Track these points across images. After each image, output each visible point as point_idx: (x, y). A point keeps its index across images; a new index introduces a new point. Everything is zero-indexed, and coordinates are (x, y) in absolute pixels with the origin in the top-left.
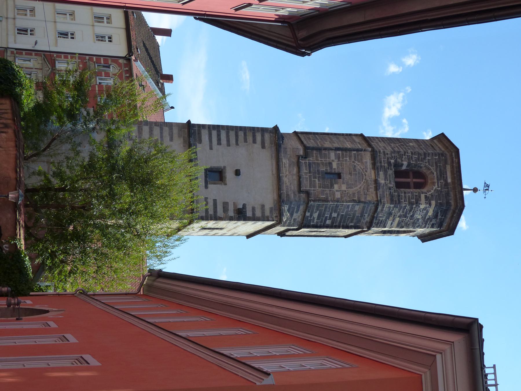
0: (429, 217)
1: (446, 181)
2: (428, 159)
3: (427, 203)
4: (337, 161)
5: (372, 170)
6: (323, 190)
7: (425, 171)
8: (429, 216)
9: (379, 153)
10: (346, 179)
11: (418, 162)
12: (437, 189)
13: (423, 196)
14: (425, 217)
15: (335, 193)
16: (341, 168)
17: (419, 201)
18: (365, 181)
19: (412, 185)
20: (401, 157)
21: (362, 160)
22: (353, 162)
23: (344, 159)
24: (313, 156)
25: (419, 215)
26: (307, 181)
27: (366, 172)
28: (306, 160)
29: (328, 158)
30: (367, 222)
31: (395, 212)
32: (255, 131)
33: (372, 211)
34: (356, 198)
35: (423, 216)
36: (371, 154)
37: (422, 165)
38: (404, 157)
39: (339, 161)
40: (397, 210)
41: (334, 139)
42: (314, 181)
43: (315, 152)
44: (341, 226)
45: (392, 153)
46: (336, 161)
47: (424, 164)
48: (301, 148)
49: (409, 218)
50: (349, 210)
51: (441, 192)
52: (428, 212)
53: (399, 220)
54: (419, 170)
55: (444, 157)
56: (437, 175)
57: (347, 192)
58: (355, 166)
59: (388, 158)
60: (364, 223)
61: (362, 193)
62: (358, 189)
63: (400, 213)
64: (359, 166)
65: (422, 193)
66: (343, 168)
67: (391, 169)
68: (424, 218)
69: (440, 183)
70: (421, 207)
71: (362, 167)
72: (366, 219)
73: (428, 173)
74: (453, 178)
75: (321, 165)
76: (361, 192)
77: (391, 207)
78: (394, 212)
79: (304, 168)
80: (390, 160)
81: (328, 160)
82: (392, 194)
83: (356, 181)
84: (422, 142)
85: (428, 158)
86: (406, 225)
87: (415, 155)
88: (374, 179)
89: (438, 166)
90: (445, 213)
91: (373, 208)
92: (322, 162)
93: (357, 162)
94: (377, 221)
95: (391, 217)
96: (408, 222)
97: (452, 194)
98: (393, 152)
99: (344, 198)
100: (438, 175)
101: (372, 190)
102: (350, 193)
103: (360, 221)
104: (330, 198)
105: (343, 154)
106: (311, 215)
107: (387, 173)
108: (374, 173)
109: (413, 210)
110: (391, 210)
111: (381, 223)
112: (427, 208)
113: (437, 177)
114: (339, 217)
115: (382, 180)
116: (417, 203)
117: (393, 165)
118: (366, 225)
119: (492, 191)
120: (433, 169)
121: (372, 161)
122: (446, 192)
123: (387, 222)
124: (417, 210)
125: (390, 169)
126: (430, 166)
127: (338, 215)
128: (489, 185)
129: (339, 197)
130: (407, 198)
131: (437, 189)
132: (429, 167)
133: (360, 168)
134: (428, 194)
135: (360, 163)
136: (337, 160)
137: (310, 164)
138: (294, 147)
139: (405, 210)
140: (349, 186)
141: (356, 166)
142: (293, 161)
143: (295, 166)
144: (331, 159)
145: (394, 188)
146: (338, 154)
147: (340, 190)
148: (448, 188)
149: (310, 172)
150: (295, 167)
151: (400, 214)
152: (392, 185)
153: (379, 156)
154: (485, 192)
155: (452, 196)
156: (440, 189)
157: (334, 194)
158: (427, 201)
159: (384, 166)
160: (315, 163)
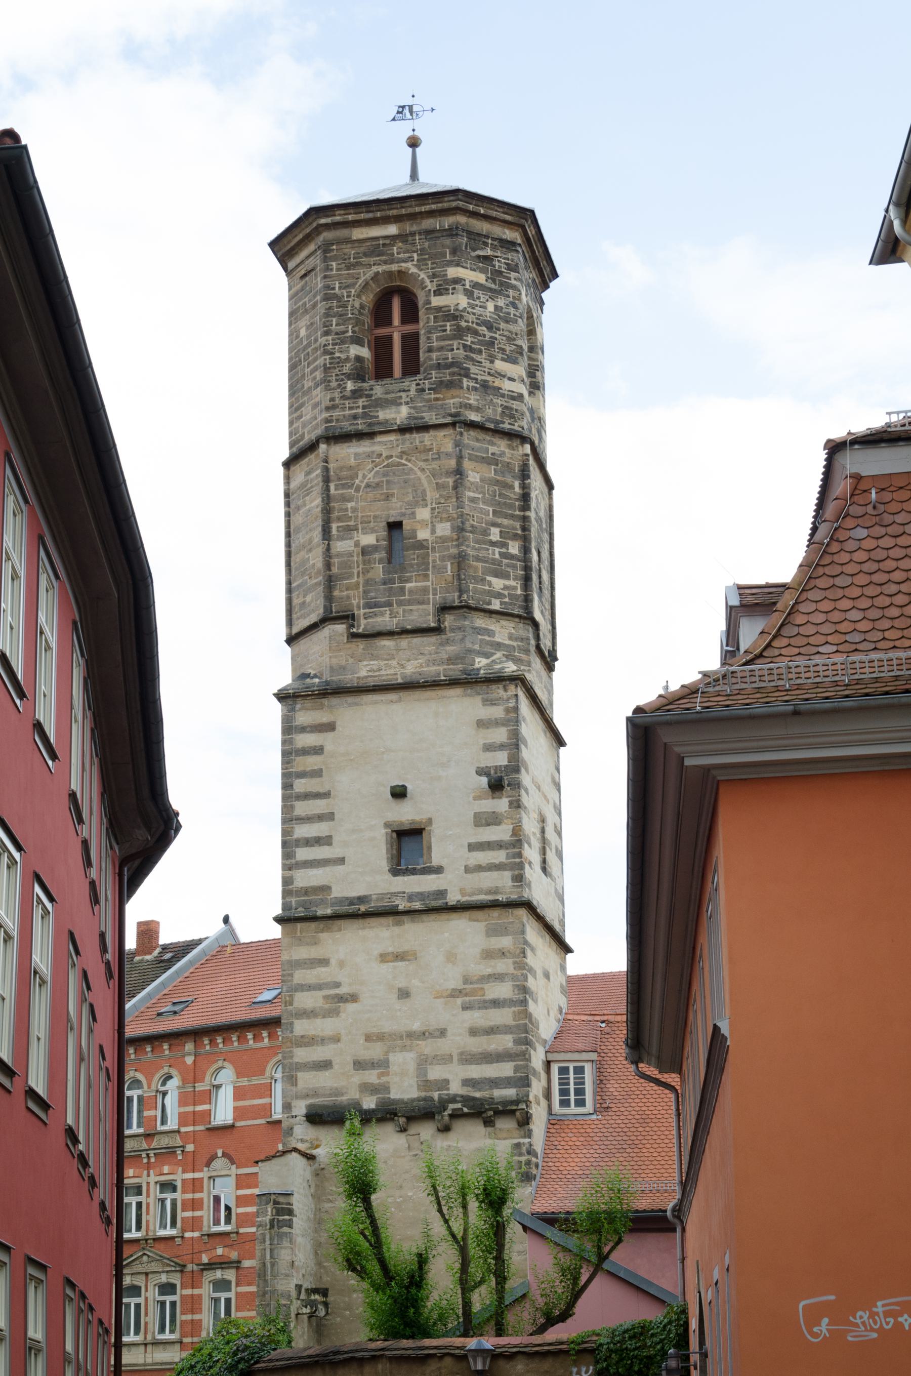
2: (340, 288)
3: (454, 289)
9: (331, 421)
11: (350, 316)
12: (415, 263)
13: (436, 301)
14: (491, 290)
15: (440, 537)
17: (450, 311)
19: (409, 328)
20: (338, 363)
24: (348, 597)
29: (351, 559)
30: (510, 447)
34: (450, 481)
37: (357, 305)
38: (337, 355)
39: (357, 529)
41: (299, 539)
43: (336, 593)
44: (522, 513)
47: (354, 300)
50: (480, 496)
51: (422, 252)
52: (476, 285)
56: (379, 264)
57: (434, 505)
58: (368, 486)
59: (344, 398)
60: (512, 455)
61: (435, 465)
65: (428, 302)
66: (375, 517)
68: (494, 294)
69: (401, 256)
71: (370, 466)
75: (370, 575)
80: (348, 393)
81: (355, 558)
82: (435, 386)
85: (337, 289)
89: (357, 263)
92: (363, 573)
95: (494, 382)
96: (505, 336)
98: (326, 386)
100: (380, 260)
102: (437, 496)
105: (339, 519)
106: (499, 595)
107: (381, 398)
109: (474, 325)
110: (476, 385)
113: (385, 262)
114: (499, 521)
115: (399, 412)
116: (455, 317)
123: (506, 393)
124: (474, 314)
125: (371, 392)
126: (359, 284)
127: (495, 525)
128: (400, 107)
134: (429, 287)
137: (368, 606)
138: (328, 648)
139: (473, 346)
141: (367, 483)
144: (352, 548)
145: (420, 380)
146: (338, 531)
149: (389, 604)
151: (485, 359)
153: (337, 420)
156: (415, 255)
157: (443, 539)
158: (447, 289)
159: (364, 407)
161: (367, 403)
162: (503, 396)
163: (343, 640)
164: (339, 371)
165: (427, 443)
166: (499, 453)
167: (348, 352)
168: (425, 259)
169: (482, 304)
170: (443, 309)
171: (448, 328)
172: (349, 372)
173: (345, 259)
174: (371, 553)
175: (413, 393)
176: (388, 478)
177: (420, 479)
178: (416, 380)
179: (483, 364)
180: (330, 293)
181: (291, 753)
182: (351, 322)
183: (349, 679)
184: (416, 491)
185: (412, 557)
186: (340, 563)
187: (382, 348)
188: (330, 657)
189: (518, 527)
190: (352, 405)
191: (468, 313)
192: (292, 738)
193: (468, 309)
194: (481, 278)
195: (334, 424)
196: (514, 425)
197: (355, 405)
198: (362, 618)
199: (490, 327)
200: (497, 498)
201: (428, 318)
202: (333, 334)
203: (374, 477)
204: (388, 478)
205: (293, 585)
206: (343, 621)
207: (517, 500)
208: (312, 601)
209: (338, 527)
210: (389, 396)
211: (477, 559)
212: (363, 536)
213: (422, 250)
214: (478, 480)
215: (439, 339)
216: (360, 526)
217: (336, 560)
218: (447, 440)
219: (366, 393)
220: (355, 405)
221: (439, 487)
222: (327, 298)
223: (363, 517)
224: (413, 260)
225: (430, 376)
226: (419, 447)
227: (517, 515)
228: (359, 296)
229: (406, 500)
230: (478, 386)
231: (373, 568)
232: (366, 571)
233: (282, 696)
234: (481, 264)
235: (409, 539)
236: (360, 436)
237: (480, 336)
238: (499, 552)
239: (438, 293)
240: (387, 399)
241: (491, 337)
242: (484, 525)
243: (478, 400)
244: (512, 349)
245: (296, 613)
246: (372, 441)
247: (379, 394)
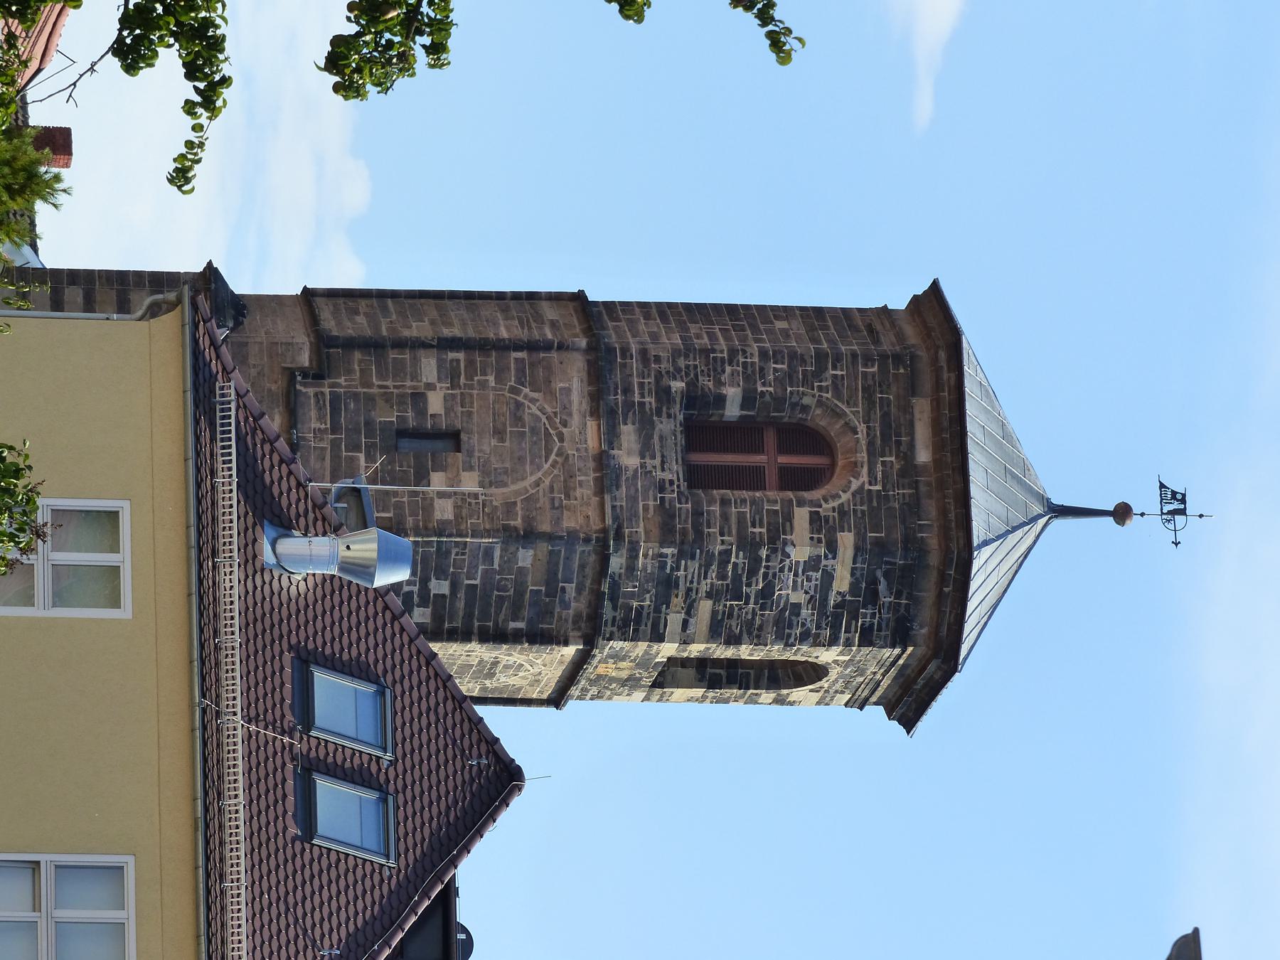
0: (840, 599)
1: (907, 456)
2: (835, 376)
3: (819, 541)
4: (448, 388)
5: (588, 418)
6: (387, 493)
7: (823, 423)
8: (839, 593)
9: (624, 356)
10: (480, 451)
11: (789, 389)
12: (867, 487)
13: (801, 516)
14: (825, 600)
15: (432, 505)
16: (462, 412)
17: (784, 533)
18: (560, 460)
19: (771, 476)
20: (715, 370)
21: (548, 381)
22: (514, 390)
23: (476, 378)
24: (349, 371)
25: (795, 588)
26: (324, 459)
27: (565, 424)
28: (323, 386)
29: (408, 377)
30: (578, 617)
31: (689, 577)
32: (129, 285)
33: (589, 571)
34: (518, 522)
35: (812, 593)
36: (588, 362)
37: (806, 401)
38: (728, 369)
39: (452, 388)
40: (694, 566)
41: (456, 312)
42: (352, 460)
43: (357, 355)
44: (476, 631)
45: (676, 353)
46: (441, 388)
47: (814, 396)
48: (302, 339)
49: (752, 600)
50: (496, 566)
51: (883, 497)
52: (828, 577)
53: (713, 612)
54: (801, 419)
55: (905, 369)
56: (868, 434)
57: (481, 498)
58: (519, 405)
59: (659, 375)
60: (566, 620)
61: (544, 502)
62: (529, 488)
63: (709, 581)
64: (535, 406)
65: (801, 503)
66: (470, 414)
67: (669, 416)
68: (819, 600)
69: (879, 467)
70: (792, 557)
71: (549, 409)
72: (573, 604)
73: (833, 429)
74: (938, 447)
75: (380, 402)
76: (541, 501)
77: (666, 556)
78: (686, 577)
79: (313, 414)
80: (665, 381)
81: (408, 383)
82: (667, 506)
83: (521, 459)
84: (832, 317)
85: (834, 372)
86: (750, 633)
87: (775, 363)
88: (596, 452)
89: (874, 403)
90: (905, 580)
91: (593, 558)
92: (386, 393)
93: (528, 390)
94: (619, 615)
95: (677, 596)
96: (753, 618)
97: (931, 508)
98: (680, 350)
99: (469, 522)
100: (875, 435)
101: (585, 490)
102: (495, 503)
103: (552, 613)
104: (410, 521)
105: (470, 363)
107: (654, 429)
108: (595, 428)
109: (762, 570)
110: (669, 567)
111: (638, 621)
112: (824, 562)
113: (871, 444)
114: (461, 594)
115: (629, 453)
116: (773, 539)
117: (678, 400)
118: (579, 629)
119: (1201, 516)
120: (853, 414)
121: (590, 384)
122: (907, 500)
123: (663, 616)
124: (782, 570)
125: (664, 415)
126: (840, 404)
127: (454, 587)
128: (1184, 495)
129: (449, 515)
130: (733, 520)
131: (867, 487)
132: (836, 405)
133: (539, 413)
134: (824, 505)
135: (541, 394)
136: (449, 385)
137: (335, 399)
138: (275, 340)
139: (730, 567)
140: (490, 478)
141: (523, 404)
142: (270, 390)
143: (278, 406)
144: (424, 380)
145: (678, 486)
146: (452, 361)
147: (455, 493)
148: (915, 485)
149: (335, 429)
150: (276, 410)
151: (712, 584)
152: (674, 472)
153: (624, 366)
154: (1169, 521)
155: (933, 512)
156: (878, 487)
157: (428, 508)
158: (819, 532)
159: (642, 404)
160: (356, 396)
161: (647, 410)
162: (657, 610)
163: (285, 362)
164: (702, 371)
165: (578, 492)
166: (567, 598)
167: (732, 385)
168: (870, 501)
169: (800, 583)
170: (788, 524)
171: (757, 530)
172: (700, 385)
173: (880, 386)
174: (415, 405)
175: (659, 475)
176: (528, 434)
177: (523, 479)
178: (679, 480)
179: (704, 582)
180: (828, 362)
181: (122, 284)
182: (779, 390)
184: (506, 472)
185: (405, 463)
186: (403, 361)
188: (261, 343)
189: (455, 625)
190: (646, 388)
191: (782, 561)
192: (145, 286)
193: (788, 560)
194: (842, 583)
195: (619, 360)
196: (613, 625)
197: (646, 391)
198: (318, 389)
200: (496, 592)
201: (777, 502)
202: (762, 364)
203: (532, 414)
204: (528, 434)
205: (389, 302)
206: (314, 363)
207: (496, 623)
208: (355, 323)
209: (458, 361)
210: (656, 438)
212: (443, 395)
213: (887, 497)
214: (520, 564)
215: (741, 516)
216: (457, 392)
217: (407, 356)
218: (581, 520)
219: (664, 409)
220: (646, 391)
221: (510, 507)
222: (820, 357)
223: (471, 396)
224: (870, 484)
225: (683, 500)
226: (573, 480)
227: (473, 626)
228: (820, 403)
229: (493, 459)
230: (668, 571)
231: (392, 407)
232: (387, 398)
234: (864, 585)
235: (432, 461)
237: (747, 579)
238: (412, 592)
239: (815, 519)
240: (651, 437)
241: (748, 597)
242: (452, 570)
243: (645, 569)
244: (734, 628)
245: (345, 303)
246: (588, 414)
247: (661, 426)
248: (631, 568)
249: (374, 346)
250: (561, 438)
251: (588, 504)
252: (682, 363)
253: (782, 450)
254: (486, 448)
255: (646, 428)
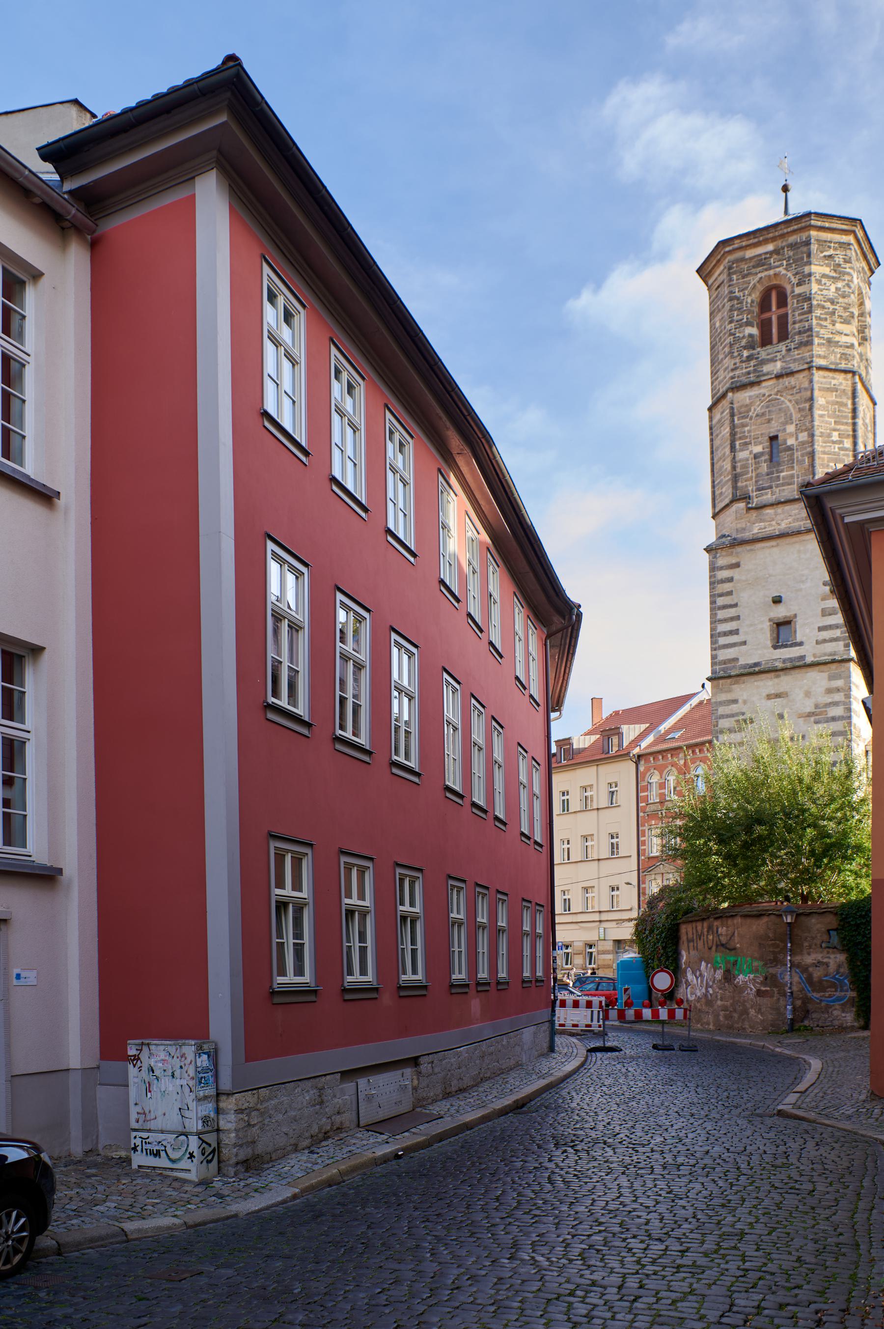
1: (771, 253)
6: (797, 461)
14: (833, 277)
15: (801, 442)
19: (782, 311)
21: (747, 405)
27: (764, 395)
34: (807, 405)
37: (749, 301)
38: (737, 335)
39: (751, 443)
40: (822, 331)
42: (784, 478)
43: (739, 484)
45: (733, 357)
52: (824, 276)
57: (797, 422)
58: (757, 415)
59: (742, 362)
61: (798, 397)
64: (757, 409)
65: (793, 292)
66: (762, 434)
68: (835, 279)
69: (776, 264)
71: (758, 403)
73: (760, 288)
79: (765, 497)
80: (744, 359)
81: (750, 462)
104: (809, 449)
105: (740, 438)
112: (817, 277)
113: (766, 270)
114: (838, 427)
115: (775, 366)
127: (835, 430)
129: (806, 434)
137: (758, 490)
140: (789, 420)
149: (771, 487)
152: (782, 347)
158: (805, 281)
159: (754, 366)
160: (756, 482)
167: (744, 332)
174: (759, 457)
175: (784, 352)
177: (788, 407)
183: (747, 535)
187: (765, 327)
194: (827, 270)
199: (832, 302)
211: (824, 453)
215: (800, 315)
216: (753, 442)
221: (800, 410)
229: (780, 421)
233: (708, 550)
236: (752, 384)
248: (825, 357)
249: (735, 478)
250: (770, 395)
251: (798, 378)
252: (736, 354)
253: (770, 309)
254: (776, 425)
255: (763, 362)
